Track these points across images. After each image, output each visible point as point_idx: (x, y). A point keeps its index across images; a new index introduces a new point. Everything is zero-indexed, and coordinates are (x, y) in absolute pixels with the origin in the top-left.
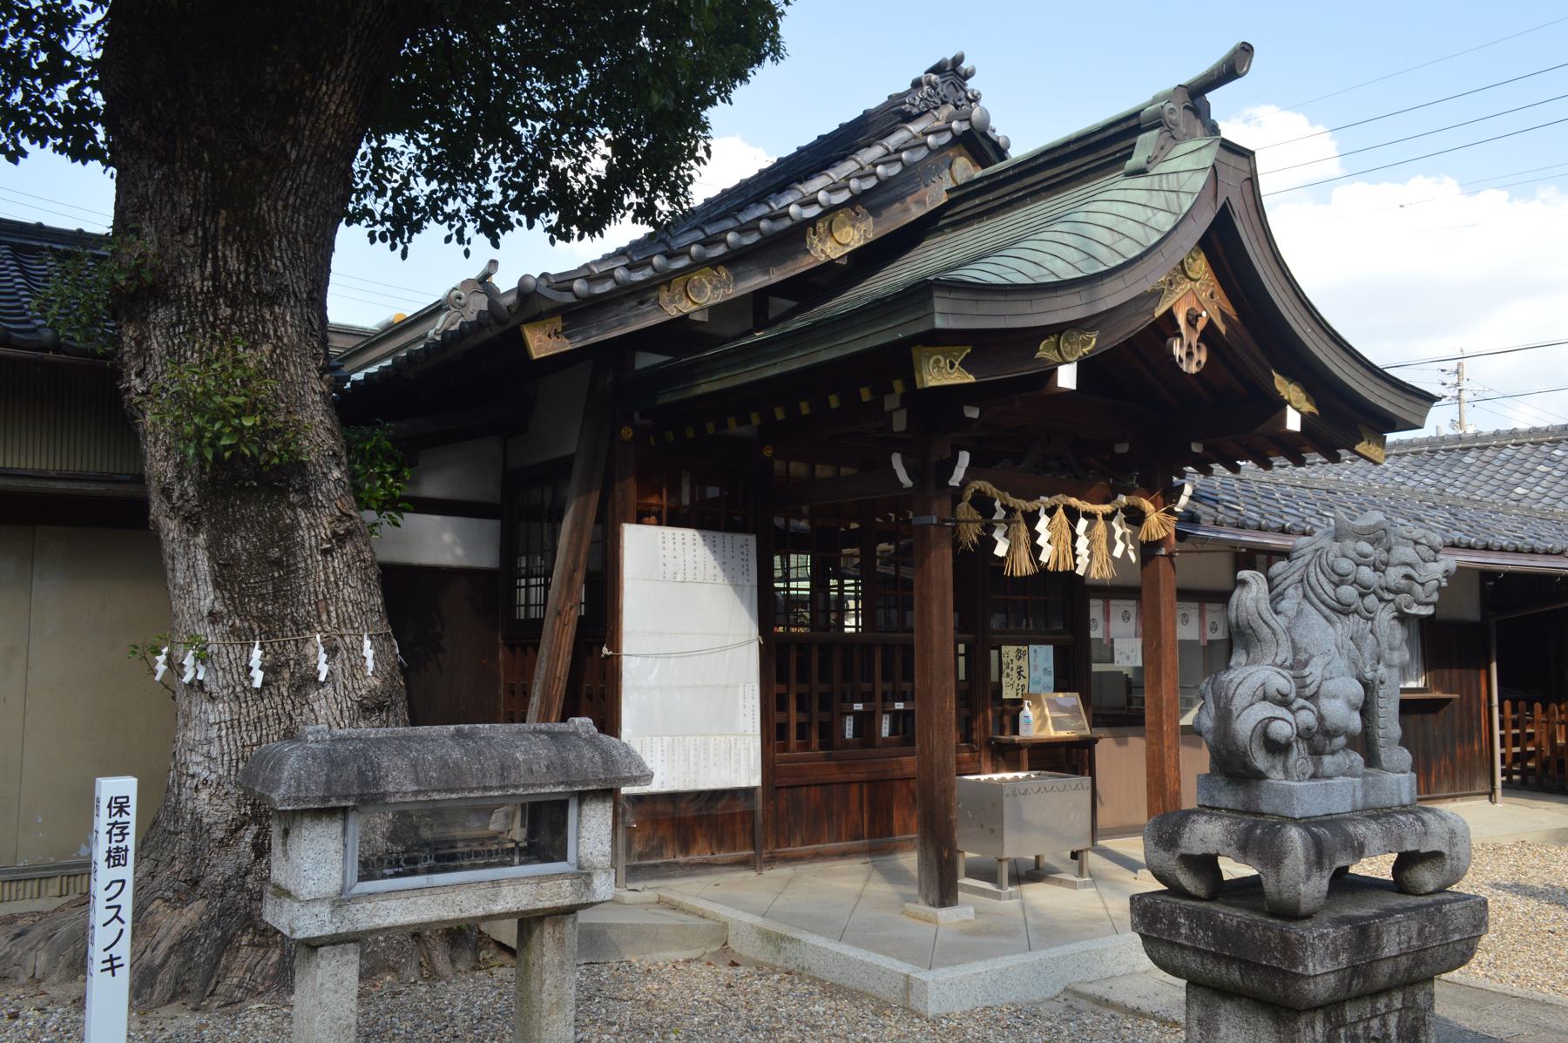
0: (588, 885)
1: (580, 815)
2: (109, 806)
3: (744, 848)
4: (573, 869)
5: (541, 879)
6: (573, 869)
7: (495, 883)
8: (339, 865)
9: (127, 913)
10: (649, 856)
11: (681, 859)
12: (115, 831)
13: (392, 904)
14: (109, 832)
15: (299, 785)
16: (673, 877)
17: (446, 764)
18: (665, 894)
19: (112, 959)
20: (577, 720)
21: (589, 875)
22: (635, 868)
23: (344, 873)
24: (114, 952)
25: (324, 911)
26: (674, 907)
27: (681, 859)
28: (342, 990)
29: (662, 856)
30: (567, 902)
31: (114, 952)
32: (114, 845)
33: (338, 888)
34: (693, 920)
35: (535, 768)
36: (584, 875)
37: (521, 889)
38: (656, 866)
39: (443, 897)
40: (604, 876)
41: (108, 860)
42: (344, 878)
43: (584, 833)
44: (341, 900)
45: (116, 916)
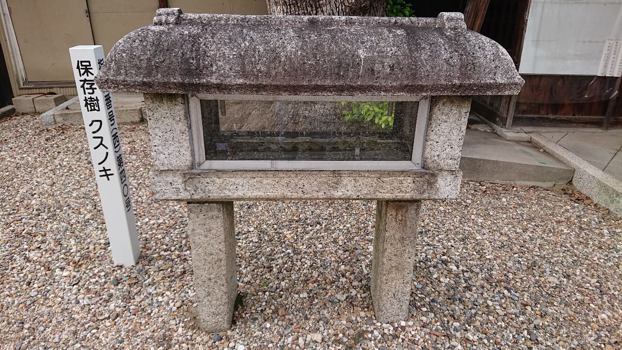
0: (431, 184)
1: (430, 118)
2: (78, 67)
3: (597, 114)
4: (417, 168)
5: (381, 174)
6: (417, 168)
7: (336, 173)
8: (186, 144)
9: (108, 141)
10: (530, 112)
11: (551, 116)
12: (86, 86)
13: (239, 180)
14: (83, 86)
15: (119, 68)
16: (543, 126)
17: (277, 57)
18: (536, 138)
19: (105, 170)
20: (446, 15)
21: (433, 175)
22: (519, 118)
23: (193, 151)
24: (106, 165)
25: (178, 180)
26: (536, 146)
27: (551, 116)
28: (211, 235)
29: (539, 113)
30: (408, 196)
31: (106, 165)
32: (88, 96)
33: (188, 163)
34: (550, 164)
35: (377, 67)
36: (428, 174)
37: (361, 181)
38: (533, 119)
39: (286, 180)
40: (450, 178)
41: (86, 105)
42: (193, 155)
43: (432, 136)
44: (191, 174)
45: (101, 144)
